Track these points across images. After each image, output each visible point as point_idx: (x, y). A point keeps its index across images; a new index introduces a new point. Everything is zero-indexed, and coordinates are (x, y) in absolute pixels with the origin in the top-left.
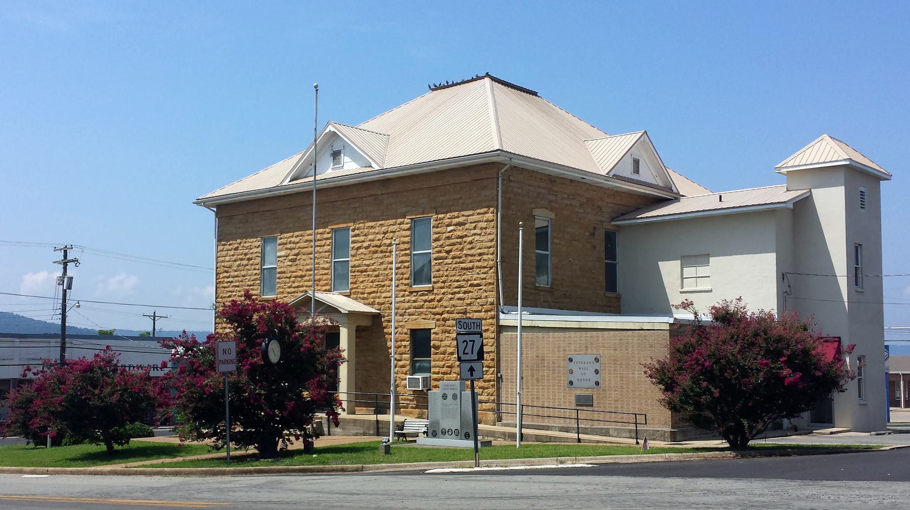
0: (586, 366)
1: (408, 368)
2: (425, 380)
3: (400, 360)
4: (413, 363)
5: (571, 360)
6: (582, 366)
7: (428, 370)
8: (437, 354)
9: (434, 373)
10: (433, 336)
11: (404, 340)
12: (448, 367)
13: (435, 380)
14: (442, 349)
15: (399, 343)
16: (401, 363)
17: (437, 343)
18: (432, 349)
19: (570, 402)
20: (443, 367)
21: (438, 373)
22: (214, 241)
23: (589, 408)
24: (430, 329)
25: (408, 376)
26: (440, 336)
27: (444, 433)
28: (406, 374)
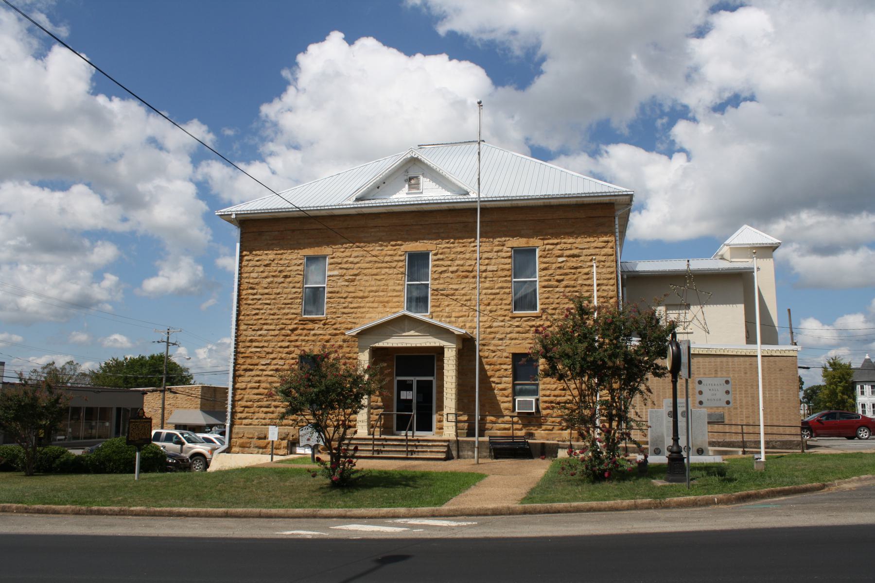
4: (514, 385)
5: (700, 382)
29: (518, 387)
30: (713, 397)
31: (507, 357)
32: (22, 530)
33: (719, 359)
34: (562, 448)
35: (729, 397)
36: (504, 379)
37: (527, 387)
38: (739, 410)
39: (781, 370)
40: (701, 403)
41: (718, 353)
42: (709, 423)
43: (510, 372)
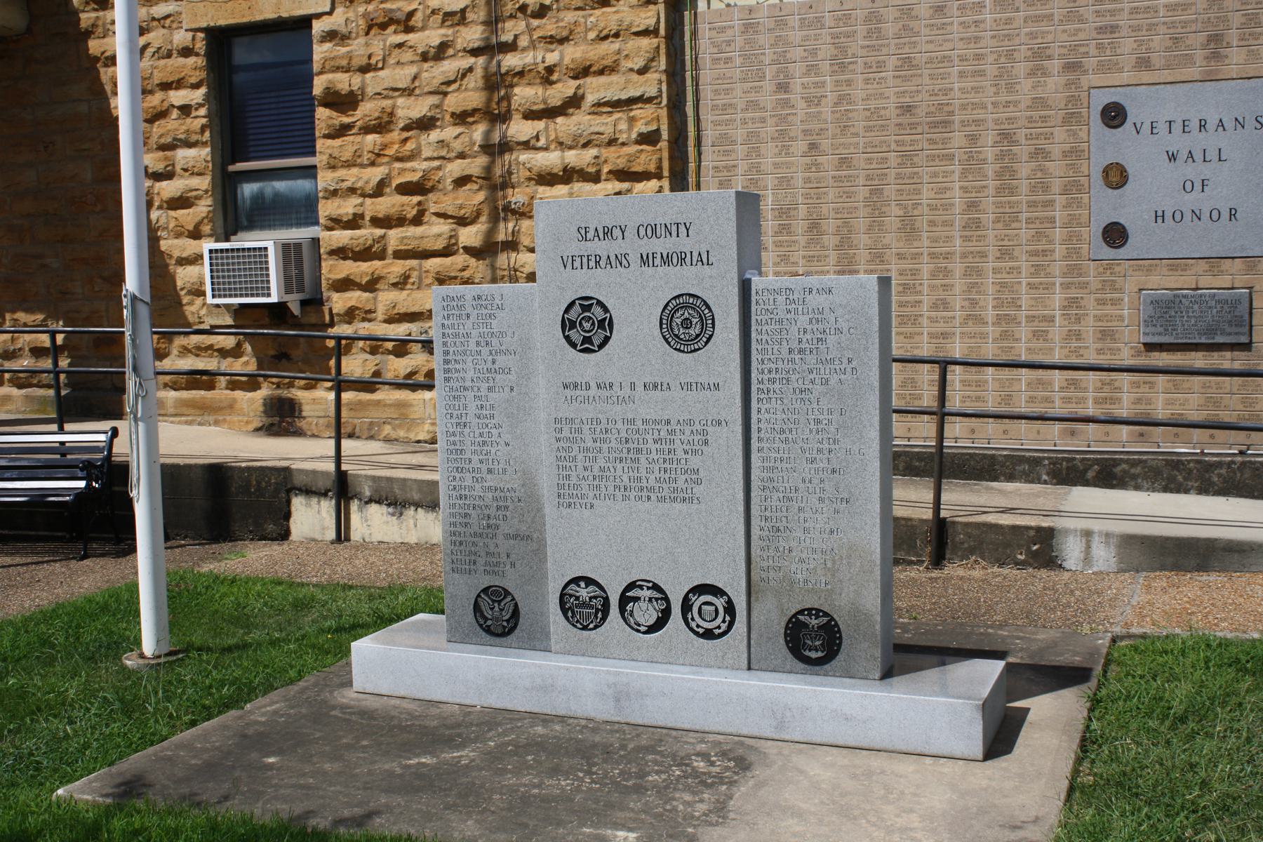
0: (1211, 140)
1: (203, 208)
2: (290, 252)
3: (168, 175)
4: (226, 184)
5: (1114, 115)
6: (1178, 142)
7: (304, 211)
8: (341, 131)
9: (336, 223)
10: (320, 51)
11: (178, 84)
12: (406, 189)
13: (341, 253)
14: (367, 110)
15: (156, 100)
16: (168, 189)
17: (343, 82)
18: (322, 113)
19: (1106, 335)
20: (379, 191)
21: (354, 223)
22: (892, 549)
23: (1225, 361)
24: (304, 23)
25: (207, 245)
26: (358, 48)
27: (586, 606)
28: (196, 234)
29: (248, 189)
30: (1192, 200)
31: (186, 52)
34: (308, 492)
36: (184, 155)
37: (281, 186)
40: (1115, 235)
42: (679, 182)
43: (199, 119)
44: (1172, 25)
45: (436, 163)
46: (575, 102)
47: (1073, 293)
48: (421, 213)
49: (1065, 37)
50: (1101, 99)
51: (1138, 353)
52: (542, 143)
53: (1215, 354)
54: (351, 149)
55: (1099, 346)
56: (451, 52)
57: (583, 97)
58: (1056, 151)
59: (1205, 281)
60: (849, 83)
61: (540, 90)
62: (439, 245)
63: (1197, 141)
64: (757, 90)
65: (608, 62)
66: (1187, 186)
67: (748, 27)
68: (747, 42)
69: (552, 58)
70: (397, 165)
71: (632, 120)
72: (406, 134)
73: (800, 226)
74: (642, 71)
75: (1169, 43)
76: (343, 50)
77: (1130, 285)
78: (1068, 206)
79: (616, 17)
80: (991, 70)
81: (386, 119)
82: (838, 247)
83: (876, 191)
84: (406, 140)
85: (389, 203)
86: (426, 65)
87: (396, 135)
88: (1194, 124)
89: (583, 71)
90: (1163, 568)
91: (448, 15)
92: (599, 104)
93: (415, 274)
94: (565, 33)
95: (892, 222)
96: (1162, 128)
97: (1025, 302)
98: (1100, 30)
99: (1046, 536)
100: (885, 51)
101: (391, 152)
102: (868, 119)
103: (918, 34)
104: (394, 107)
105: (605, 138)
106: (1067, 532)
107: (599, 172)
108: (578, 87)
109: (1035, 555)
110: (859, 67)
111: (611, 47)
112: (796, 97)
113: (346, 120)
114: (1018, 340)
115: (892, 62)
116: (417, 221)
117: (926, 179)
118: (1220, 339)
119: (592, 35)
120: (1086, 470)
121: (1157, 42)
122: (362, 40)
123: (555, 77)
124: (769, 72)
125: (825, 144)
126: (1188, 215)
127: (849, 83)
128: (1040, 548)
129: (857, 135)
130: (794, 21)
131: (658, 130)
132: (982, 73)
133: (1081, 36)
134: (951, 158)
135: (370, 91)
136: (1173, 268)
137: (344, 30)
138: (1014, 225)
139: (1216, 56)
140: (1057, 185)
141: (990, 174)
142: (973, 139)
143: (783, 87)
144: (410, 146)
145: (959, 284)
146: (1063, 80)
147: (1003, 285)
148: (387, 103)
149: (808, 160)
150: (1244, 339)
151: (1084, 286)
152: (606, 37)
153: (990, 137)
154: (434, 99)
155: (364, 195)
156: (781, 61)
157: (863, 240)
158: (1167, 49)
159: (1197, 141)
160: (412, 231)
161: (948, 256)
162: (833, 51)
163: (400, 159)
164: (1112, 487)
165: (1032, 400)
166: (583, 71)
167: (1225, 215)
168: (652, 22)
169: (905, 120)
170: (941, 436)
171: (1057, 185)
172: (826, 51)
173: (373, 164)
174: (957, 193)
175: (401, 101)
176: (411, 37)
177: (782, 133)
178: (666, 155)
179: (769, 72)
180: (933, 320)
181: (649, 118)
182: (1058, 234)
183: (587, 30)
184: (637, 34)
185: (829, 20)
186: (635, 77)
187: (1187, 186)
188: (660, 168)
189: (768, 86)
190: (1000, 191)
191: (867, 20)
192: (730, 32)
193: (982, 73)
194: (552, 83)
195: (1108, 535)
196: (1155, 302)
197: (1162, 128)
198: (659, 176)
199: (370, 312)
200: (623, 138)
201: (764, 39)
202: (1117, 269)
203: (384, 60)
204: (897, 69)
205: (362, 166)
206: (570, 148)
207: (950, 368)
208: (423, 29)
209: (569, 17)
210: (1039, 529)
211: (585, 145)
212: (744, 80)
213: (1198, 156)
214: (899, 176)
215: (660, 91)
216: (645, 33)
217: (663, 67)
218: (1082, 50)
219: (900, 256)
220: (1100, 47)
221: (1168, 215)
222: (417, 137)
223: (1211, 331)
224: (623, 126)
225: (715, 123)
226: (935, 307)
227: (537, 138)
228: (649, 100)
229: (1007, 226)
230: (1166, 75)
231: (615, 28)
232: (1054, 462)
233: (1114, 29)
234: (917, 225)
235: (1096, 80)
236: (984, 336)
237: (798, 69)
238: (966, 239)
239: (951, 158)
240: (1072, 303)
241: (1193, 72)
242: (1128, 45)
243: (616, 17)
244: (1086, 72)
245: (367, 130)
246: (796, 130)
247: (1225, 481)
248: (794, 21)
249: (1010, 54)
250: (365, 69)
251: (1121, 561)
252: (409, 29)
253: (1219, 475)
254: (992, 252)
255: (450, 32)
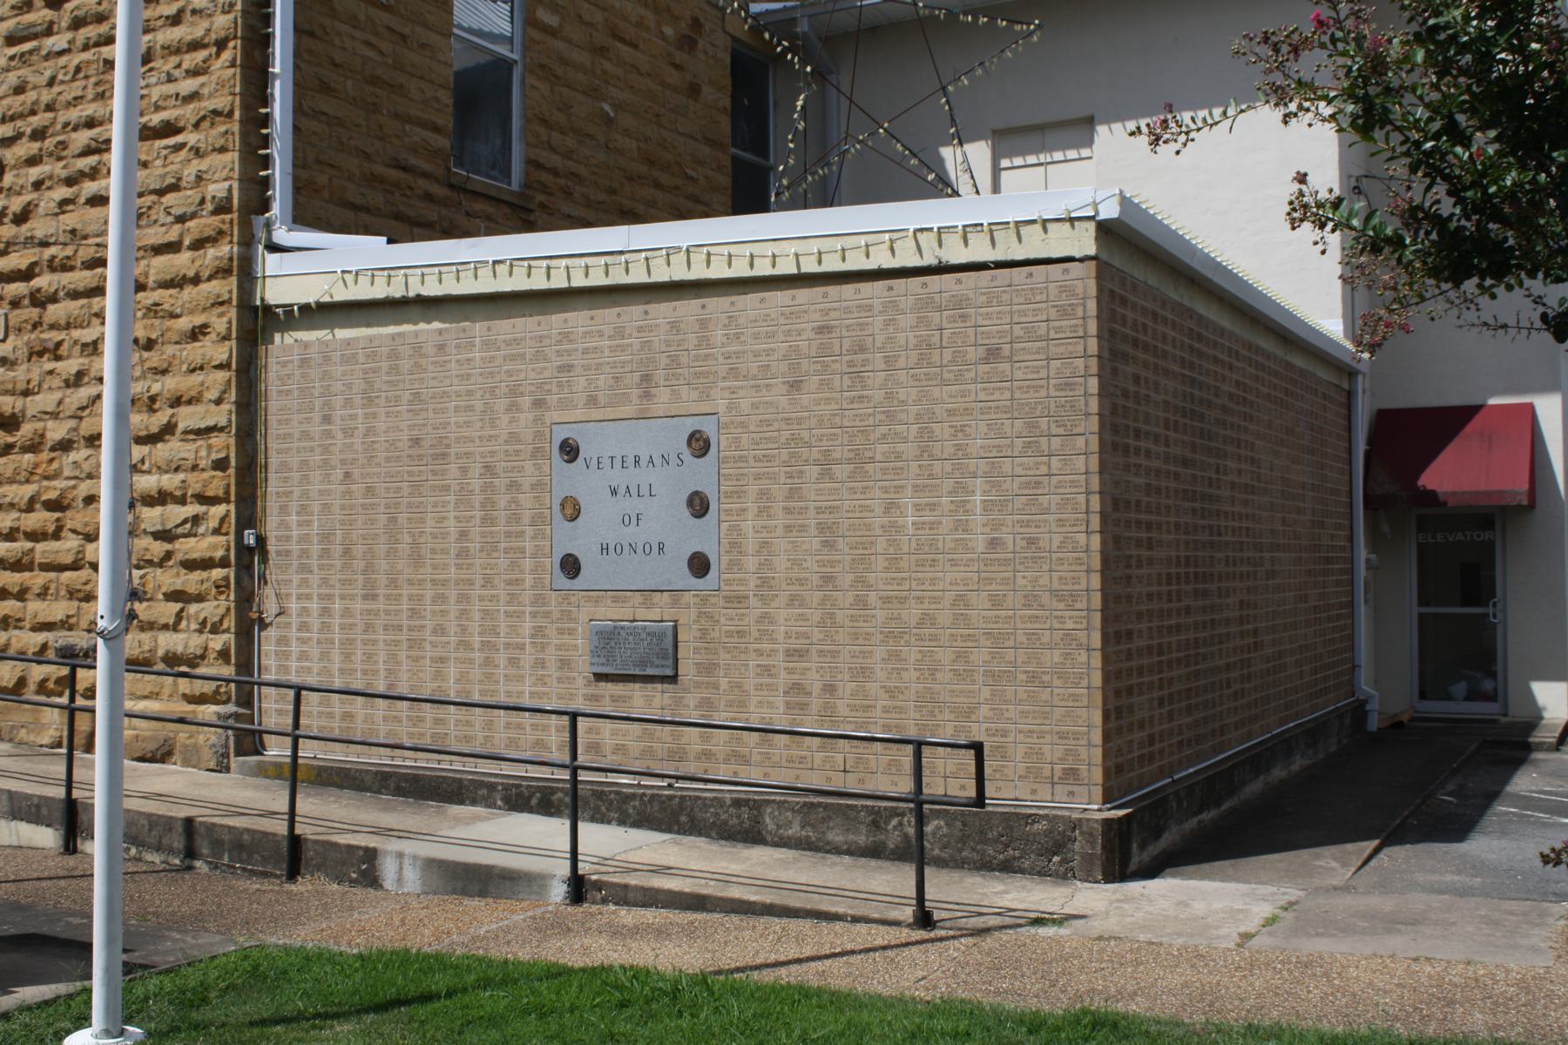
5: (570, 451)
12: (53, 506)
14: (27, 429)
30: (630, 534)
32: (641, 954)
33: (663, 311)
35: (701, 536)
38: (756, 608)
39: (993, 354)
40: (571, 566)
41: (661, 275)
44: (614, 365)
45: (72, 483)
46: (169, 429)
47: (541, 622)
48: (59, 529)
49: (533, 375)
50: (560, 434)
51: (588, 684)
52: (146, 467)
53: (649, 686)
54: (12, 467)
55: (559, 674)
56: (86, 379)
57: (176, 425)
58: (526, 483)
59: (642, 613)
60: (374, 415)
61: (145, 416)
62: (68, 559)
63: (633, 476)
64: (308, 420)
65: (193, 393)
66: (625, 521)
67: (304, 362)
68: (304, 376)
69: (156, 388)
70: (45, 483)
71: (210, 447)
72: (53, 455)
73: (337, 550)
74: (218, 402)
75: (612, 382)
76: (12, 374)
77: (583, 617)
78: (534, 538)
79: (201, 351)
80: (479, 405)
81: (37, 440)
82: (365, 572)
83: (393, 520)
84: (52, 460)
85: (40, 519)
86: (69, 391)
87: (45, 455)
88: (630, 460)
89: (177, 402)
90: (454, 892)
91: (85, 345)
92: (186, 432)
93: (53, 586)
94: (165, 365)
95: (404, 549)
96: (606, 462)
97: (503, 630)
98: (561, 369)
99: (371, 855)
100: (401, 386)
101: (39, 471)
102: (387, 450)
103: (425, 370)
104: (45, 429)
105: (189, 463)
106: (386, 852)
107: (184, 495)
108: (172, 416)
109: (363, 874)
110: (382, 402)
111: (197, 378)
112: (335, 428)
113: (10, 440)
114: (497, 666)
115: (407, 396)
116: (56, 536)
117: (430, 509)
118: (650, 671)
119: (184, 368)
120: (530, 798)
121: (603, 381)
122: (24, 366)
123: (156, 406)
124: (318, 403)
125: (356, 472)
126: (627, 548)
127: (374, 415)
128: (362, 868)
129: (379, 465)
130: (336, 356)
131: (227, 458)
132: (470, 408)
133: (546, 374)
134: (447, 488)
135: (29, 413)
136: (615, 600)
137: (11, 357)
138: (495, 554)
139: (647, 395)
140: (527, 516)
141: (477, 505)
142: (464, 471)
143: (327, 419)
144: (55, 465)
145: (453, 609)
146: (531, 416)
147: (486, 612)
148: (40, 425)
149: (342, 488)
150: (669, 672)
151: (547, 614)
152: (193, 371)
153: (476, 469)
154: (72, 423)
155: (21, 511)
156: (327, 393)
157: (383, 565)
158: (611, 388)
159: (633, 476)
160: (52, 545)
161: (444, 583)
162: (364, 386)
163: (47, 478)
164: (550, 814)
165: (546, 728)
166: (177, 402)
167: (655, 549)
168: (225, 356)
169: (415, 452)
170: (295, 756)
171: (527, 516)
172: (359, 385)
173: (28, 481)
174: (452, 522)
175: (50, 424)
176: (59, 365)
177: (326, 462)
178: (233, 481)
179: (318, 403)
180: (434, 645)
181: (224, 444)
182: (528, 563)
183: (182, 363)
184: (216, 367)
185: (361, 359)
186: (213, 407)
187: (625, 521)
188: (227, 493)
189: (317, 416)
190: (484, 520)
191: (389, 357)
192: (290, 366)
193: (470, 408)
194: (155, 411)
195: (415, 857)
196: (599, 633)
197: (606, 462)
198: (228, 501)
199: (19, 620)
200: (203, 464)
201: (314, 373)
202: (573, 599)
203: (40, 385)
204: (410, 403)
205: (21, 483)
206: (166, 472)
207: (304, 693)
208: (68, 357)
209: (170, 350)
210: (366, 849)
211: (177, 470)
212: (299, 412)
213: (634, 491)
214: (410, 505)
215: (230, 421)
216: (220, 367)
217: (233, 399)
218: (547, 387)
219: (410, 582)
220: (560, 385)
221: (611, 547)
222: (60, 457)
223: (643, 663)
224: (203, 453)
225: (279, 452)
226: (435, 632)
227: (143, 461)
228: (222, 429)
229: (489, 556)
230: (611, 413)
231: (199, 361)
232: (506, 788)
233: (570, 368)
234: (423, 552)
235: (556, 416)
236: (471, 661)
237: (338, 401)
238: (459, 567)
239: (447, 488)
240: (538, 632)
241: (628, 410)
242: (581, 383)
243: (201, 351)
244: (548, 409)
245: (26, 449)
246: (335, 459)
247: (639, 814)
248: (336, 356)
249: (493, 391)
250: (26, 393)
251: (424, 884)
252: (58, 358)
253: (634, 807)
254: (479, 581)
255: (86, 361)
